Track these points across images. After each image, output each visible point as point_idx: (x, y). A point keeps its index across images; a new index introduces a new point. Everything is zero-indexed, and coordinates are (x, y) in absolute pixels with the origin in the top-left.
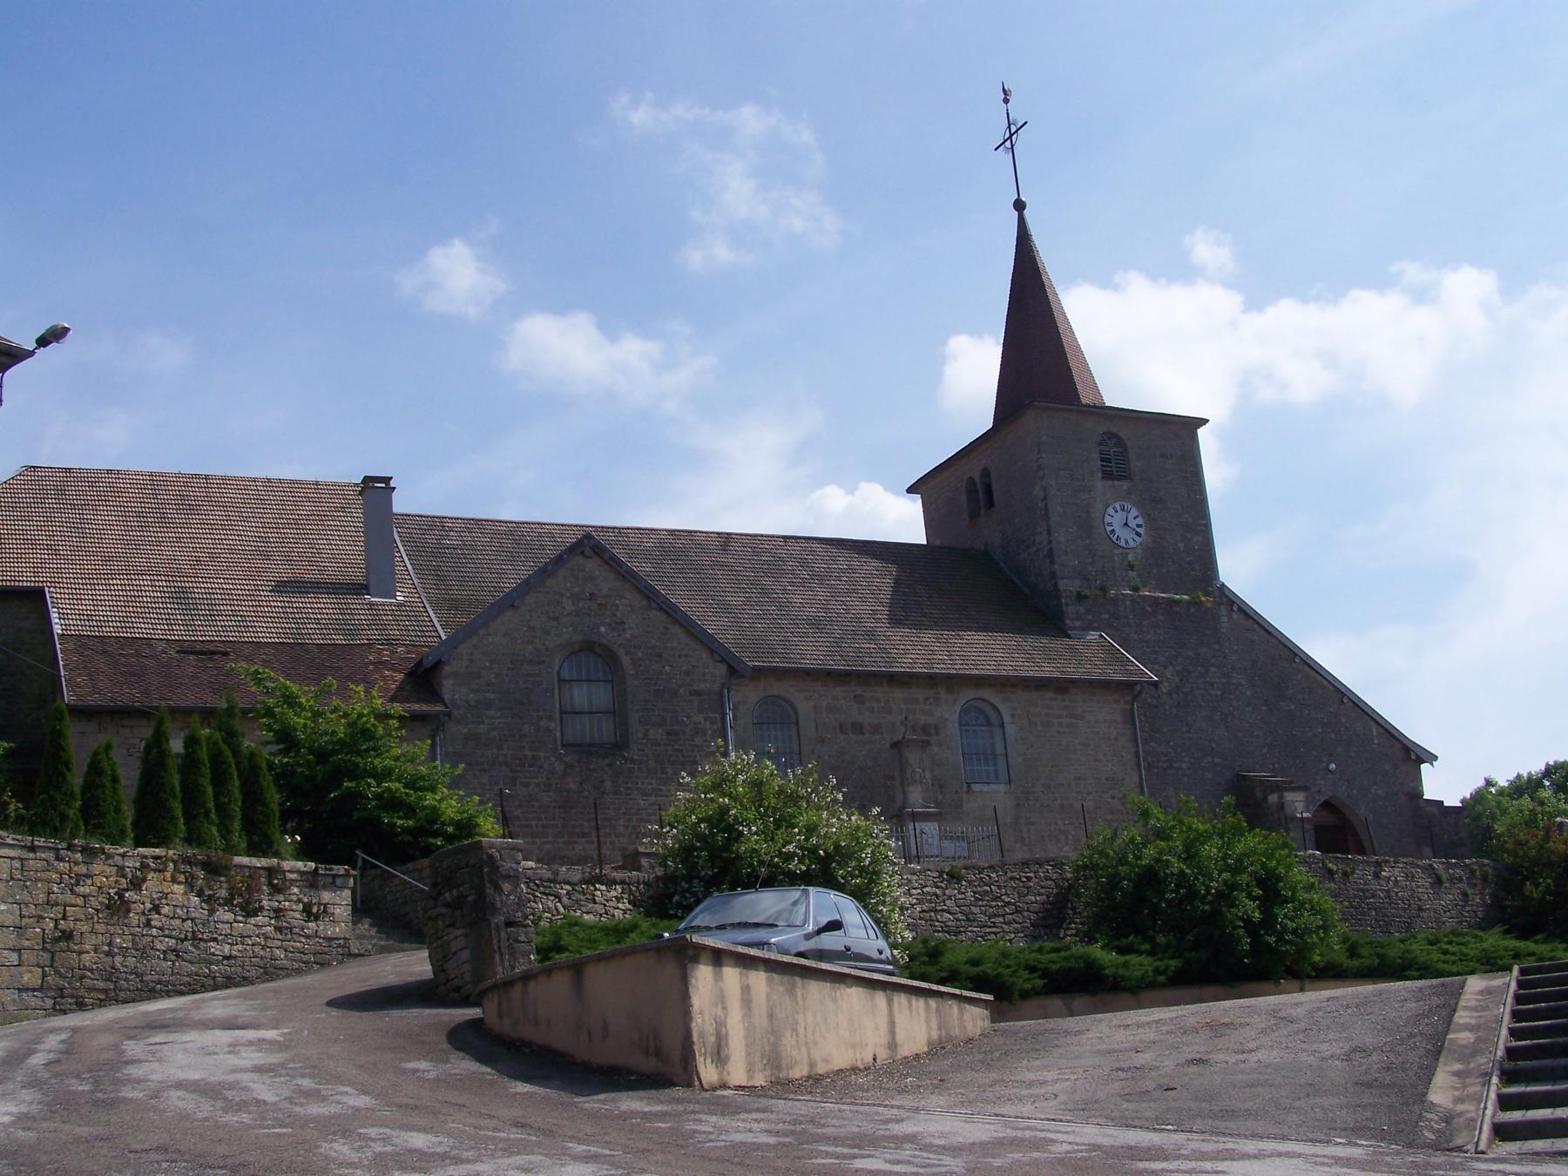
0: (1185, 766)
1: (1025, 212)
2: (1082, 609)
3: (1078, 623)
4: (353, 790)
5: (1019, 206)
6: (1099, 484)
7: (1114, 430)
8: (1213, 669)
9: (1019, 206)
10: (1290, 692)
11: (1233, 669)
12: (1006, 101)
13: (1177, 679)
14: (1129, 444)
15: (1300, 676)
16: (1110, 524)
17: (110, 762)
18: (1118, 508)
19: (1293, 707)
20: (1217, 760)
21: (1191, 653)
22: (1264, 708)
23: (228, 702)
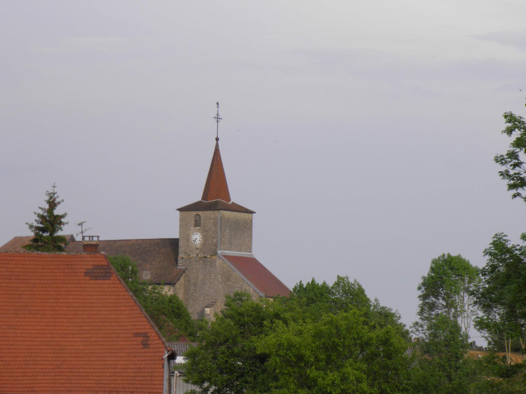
0: (201, 299)
1: (219, 141)
2: (182, 261)
3: (181, 265)
4: (481, 359)
5: (217, 139)
6: (192, 228)
7: (198, 213)
8: (213, 274)
9: (217, 139)
10: (231, 279)
11: (218, 274)
12: (218, 107)
13: (203, 277)
14: (201, 217)
15: (234, 275)
16: (200, 240)
17: (434, 368)
18: (196, 234)
19: (231, 283)
20: (210, 297)
21: (207, 271)
22: (224, 284)
23: (448, 270)
